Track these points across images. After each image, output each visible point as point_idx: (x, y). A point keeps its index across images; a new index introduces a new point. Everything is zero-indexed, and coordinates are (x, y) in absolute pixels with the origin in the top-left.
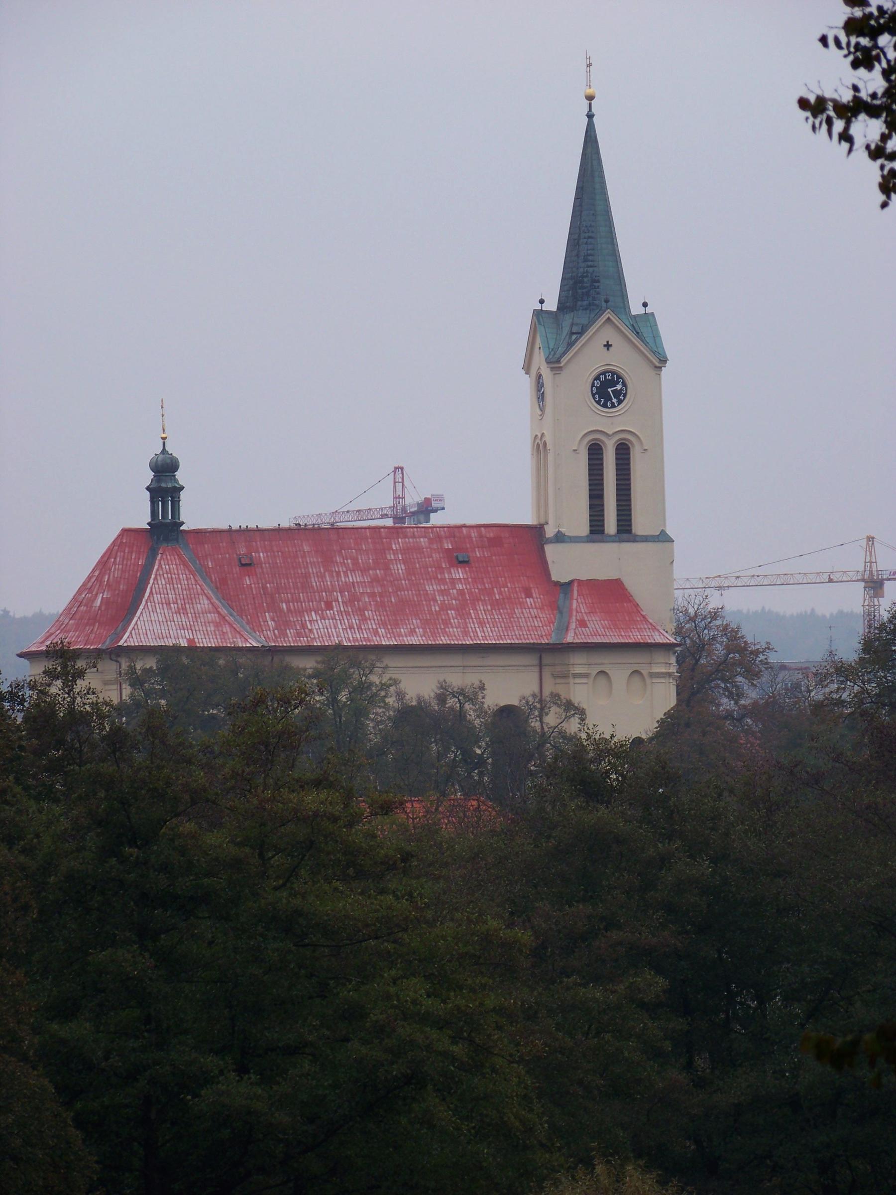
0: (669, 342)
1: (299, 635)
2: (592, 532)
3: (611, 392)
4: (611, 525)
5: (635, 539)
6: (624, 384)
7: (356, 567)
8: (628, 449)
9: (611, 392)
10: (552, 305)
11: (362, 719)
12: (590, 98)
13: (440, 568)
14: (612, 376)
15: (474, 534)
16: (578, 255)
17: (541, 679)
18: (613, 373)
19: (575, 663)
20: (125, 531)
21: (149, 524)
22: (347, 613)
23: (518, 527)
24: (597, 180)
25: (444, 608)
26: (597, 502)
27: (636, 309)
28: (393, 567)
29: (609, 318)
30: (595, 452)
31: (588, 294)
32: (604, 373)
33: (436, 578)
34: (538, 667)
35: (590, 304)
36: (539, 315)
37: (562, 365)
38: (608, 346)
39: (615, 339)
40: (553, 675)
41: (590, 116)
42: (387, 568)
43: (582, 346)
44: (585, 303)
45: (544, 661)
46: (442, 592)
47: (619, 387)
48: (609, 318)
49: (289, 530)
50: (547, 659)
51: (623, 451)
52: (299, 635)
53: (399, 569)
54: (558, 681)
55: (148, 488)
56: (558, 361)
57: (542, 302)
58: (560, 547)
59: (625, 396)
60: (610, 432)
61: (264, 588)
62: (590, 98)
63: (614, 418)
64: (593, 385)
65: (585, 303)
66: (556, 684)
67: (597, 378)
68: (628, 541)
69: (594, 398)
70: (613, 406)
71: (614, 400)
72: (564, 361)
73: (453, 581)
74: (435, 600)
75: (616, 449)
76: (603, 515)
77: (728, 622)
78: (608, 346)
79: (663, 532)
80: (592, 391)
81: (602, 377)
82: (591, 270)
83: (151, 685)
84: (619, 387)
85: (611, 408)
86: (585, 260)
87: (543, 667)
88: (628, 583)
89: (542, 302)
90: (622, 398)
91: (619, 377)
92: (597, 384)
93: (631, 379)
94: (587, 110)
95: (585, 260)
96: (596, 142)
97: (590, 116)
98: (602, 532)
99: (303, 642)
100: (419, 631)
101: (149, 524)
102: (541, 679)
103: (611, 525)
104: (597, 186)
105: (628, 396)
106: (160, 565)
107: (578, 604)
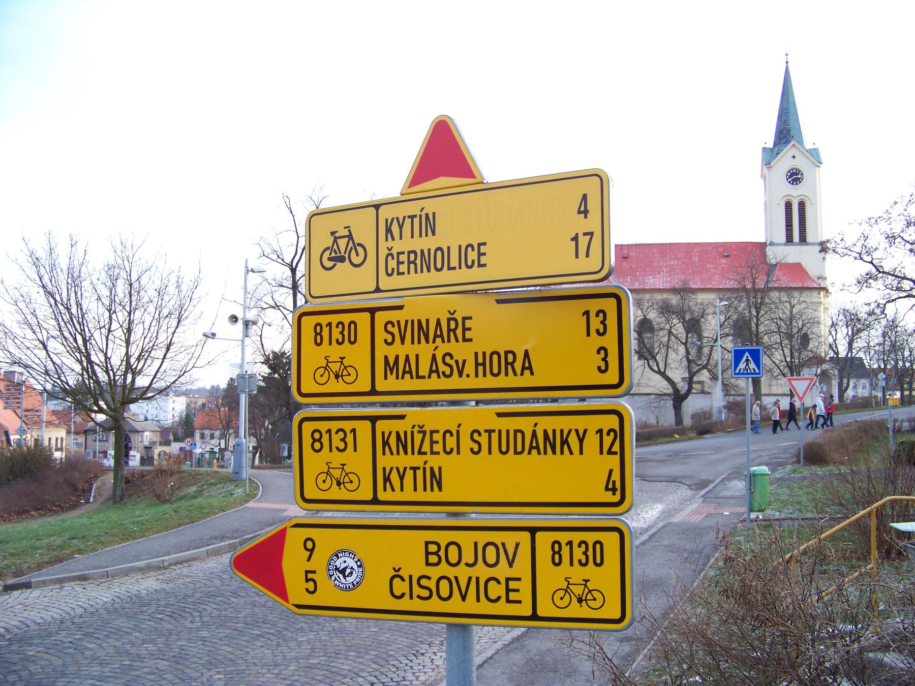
0: (823, 158)
1: (640, 284)
2: (787, 241)
4: (796, 237)
5: (808, 244)
6: (802, 174)
7: (677, 258)
8: (804, 204)
10: (770, 145)
13: (715, 259)
16: (781, 121)
17: (237, 340)
22: (666, 276)
24: (790, 89)
25: (714, 274)
26: (789, 228)
27: (808, 145)
28: (693, 258)
30: (788, 206)
32: (792, 169)
33: (713, 263)
38: (794, 157)
39: (797, 154)
42: (690, 258)
44: (784, 141)
46: (714, 268)
51: (802, 205)
52: (640, 284)
53: (696, 259)
58: (771, 247)
59: (802, 179)
60: (795, 195)
61: (631, 267)
62: (787, 62)
64: (787, 175)
65: (784, 141)
67: (789, 172)
68: (804, 245)
70: (787, 179)
71: (790, 179)
72: (772, 164)
73: (720, 264)
74: (710, 271)
75: (799, 204)
76: (792, 234)
78: (794, 157)
81: (791, 171)
84: (799, 176)
86: (784, 123)
88: (805, 265)
91: (799, 171)
92: (789, 174)
95: (784, 123)
96: (789, 73)
98: (792, 241)
99: (642, 287)
100: (699, 283)
102: (237, 340)
103: (796, 237)
105: (792, 167)
107: (777, 273)
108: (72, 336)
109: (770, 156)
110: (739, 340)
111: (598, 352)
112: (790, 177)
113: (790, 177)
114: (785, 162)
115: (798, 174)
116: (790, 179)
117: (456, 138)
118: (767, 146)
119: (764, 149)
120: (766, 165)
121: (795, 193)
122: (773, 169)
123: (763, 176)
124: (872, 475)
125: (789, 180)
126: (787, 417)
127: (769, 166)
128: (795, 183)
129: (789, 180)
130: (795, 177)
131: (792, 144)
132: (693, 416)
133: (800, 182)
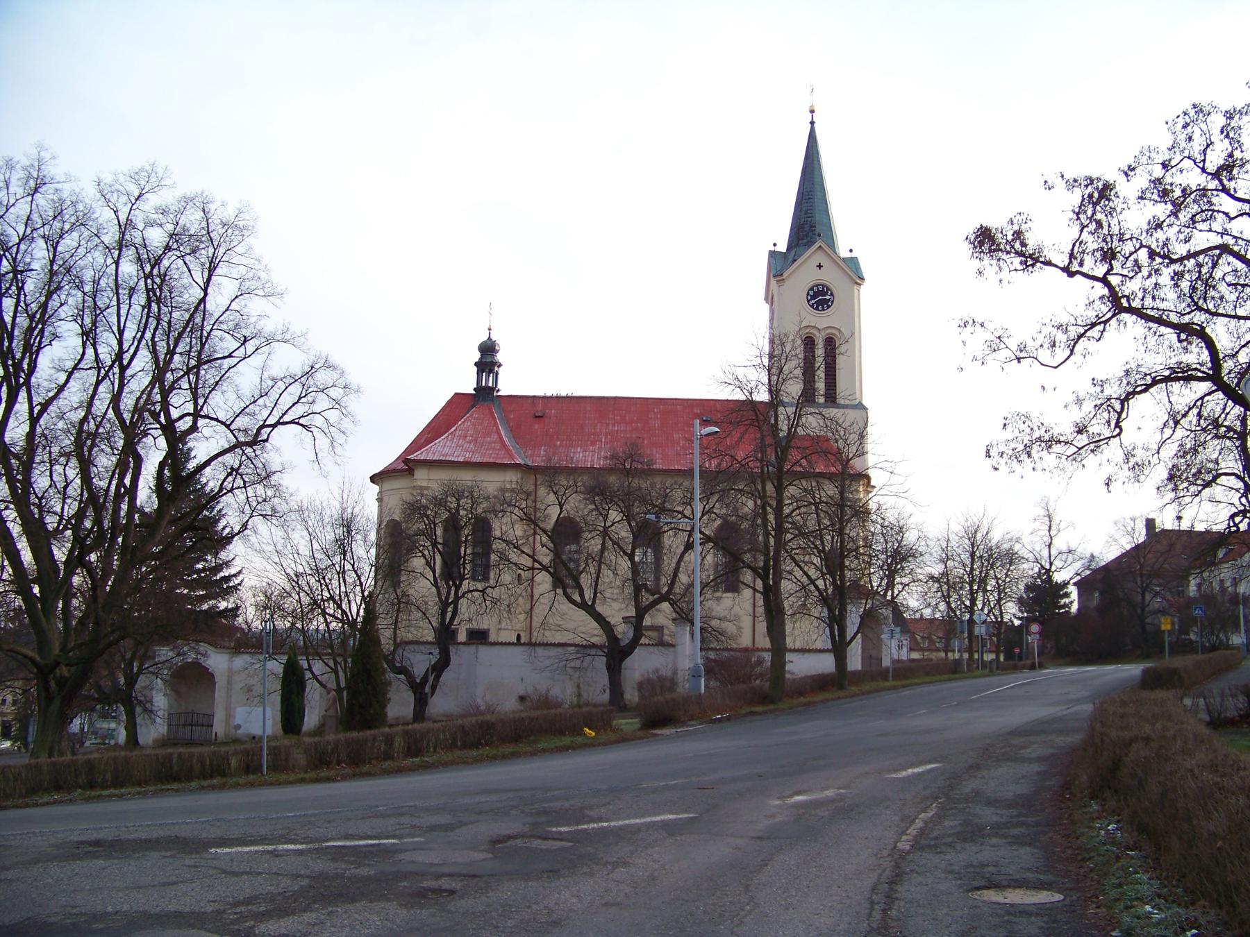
3: (1167, 644)
5: (838, 406)
6: (832, 294)
9: (1167, 644)
10: (782, 247)
15: (718, 406)
16: (801, 211)
18: (824, 286)
20: (456, 394)
21: (474, 389)
23: (804, 179)
24: (815, 162)
30: (809, 343)
31: (807, 235)
35: (808, 242)
36: (773, 254)
37: (784, 277)
38: (820, 266)
41: (812, 123)
43: (850, 276)
48: (820, 246)
49: (563, 397)
51: (830, 342)
55: (476, 364)
56: (782, 275)
57: (775, 245)
59: (832, 302)
64: (808, 294)
67: (812, 289)
70: (808, 301)
71: (813, 301)
72: (785, 275)
78: (820, 266)
79: (860, 403)
81: (815, 289)
82: (809, 219)
84: (828, 297)
89: (775, 245)
91: (828, 289)
92: (811, 293)
93: (1128, 409)
94: (810, 120)
97: (812, 123)
101: (474, 389)
104: (816, 166)
106: (472, 415)
109: (779, 265)
112: (813, 297)
113: (813, 297)
114: (806, 274)
116: (813, 301)
121: (822, 322)
122: (787, 283)
123: (769, 298)
125: (811, 303)
128: (820, 308)
129: (811, 303)
130: (820, 298)
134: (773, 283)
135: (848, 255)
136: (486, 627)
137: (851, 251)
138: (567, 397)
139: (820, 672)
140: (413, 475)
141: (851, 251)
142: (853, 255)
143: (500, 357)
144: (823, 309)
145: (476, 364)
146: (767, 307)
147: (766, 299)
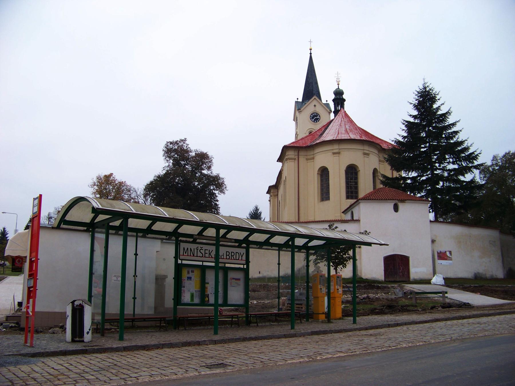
6: (319, 116)
10: (300, 100)
11: (91, 233)
12: (311, 49)
14: (316, 114)
19: (365, 149)
29: (315, 98)
32: (314, 113)
34: (297, 156)
36: (297, 102)
38: (315, 106)
40: (306, 159)
41: (311, 54)
45: (300, 154)
47: (318, 117)
48: (315, 98)
50: (302, 153)
54: (365, 156)
57: (298, 99)
59: (320, 119)
62: (311, 49)
63: (317, 125)
64: (311, 116)
66: (307, 162)
67: (312, 114)
69: (311, 120)
72: (302, 109)
77: (469, 145)
78: (315, 106)
80: (310, 118)
83: (114, 190)
84: (318, 117)
85: (316, 122)
87: (299, 156)
89: (298, 99)
90: (319, 120)
91: (318, 114)
94: (15, 229)
97: (311, 54)
108: (130, 378)
109: (299, 106)
110: (185, 148)
111: (325, 266)
112: (313, 118)
113: (313, 118)
114: (310, 108)
115: (316, 116)
117: (418, 285)
118: (299, 100)
119: (296, 102)
120: (298, 110)
122: (302, 113)
123: (295, 119)
124: (280, 279)
126: (331, 293)
127: (300, 111)
128: (315, 121)
131: (314, 98)
132: (315, 268)
133: (318, 121)
134: (297, 112)
135: (326, 102)
136: (295, 328)
137: (327, 101)
138: (282, 150)
139: (374, 278)
140: (444, 278)
141: (327, 101)
142: (328, 102)
143: (344, 96)
144: (316, 122)
145: (344, 100)
146: (294, 123)
147: (294, 120)
